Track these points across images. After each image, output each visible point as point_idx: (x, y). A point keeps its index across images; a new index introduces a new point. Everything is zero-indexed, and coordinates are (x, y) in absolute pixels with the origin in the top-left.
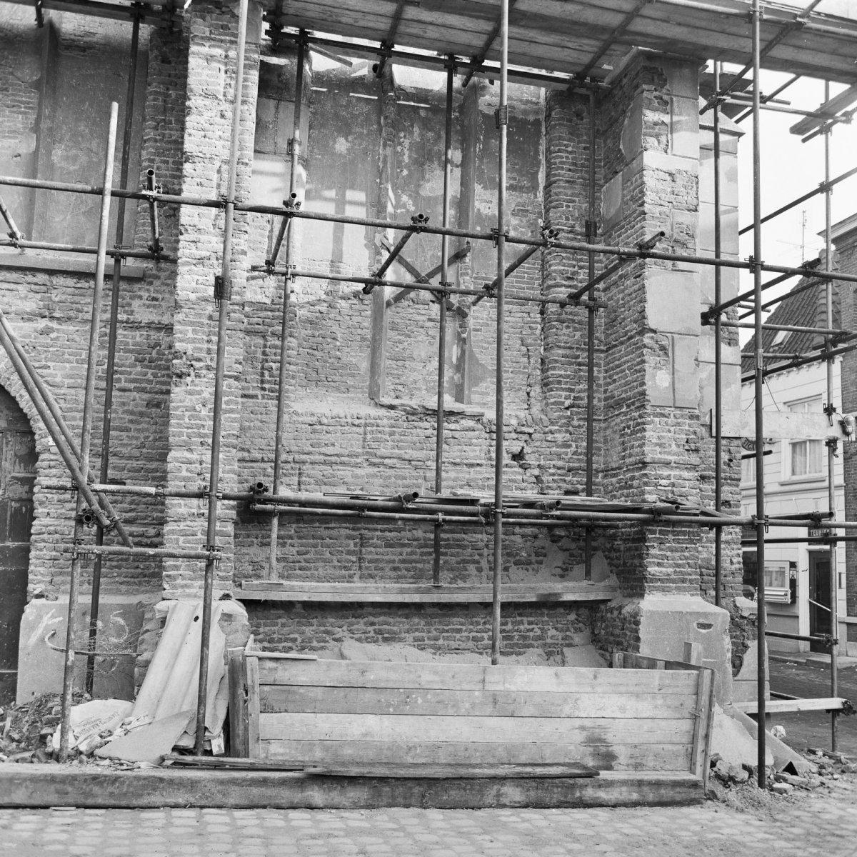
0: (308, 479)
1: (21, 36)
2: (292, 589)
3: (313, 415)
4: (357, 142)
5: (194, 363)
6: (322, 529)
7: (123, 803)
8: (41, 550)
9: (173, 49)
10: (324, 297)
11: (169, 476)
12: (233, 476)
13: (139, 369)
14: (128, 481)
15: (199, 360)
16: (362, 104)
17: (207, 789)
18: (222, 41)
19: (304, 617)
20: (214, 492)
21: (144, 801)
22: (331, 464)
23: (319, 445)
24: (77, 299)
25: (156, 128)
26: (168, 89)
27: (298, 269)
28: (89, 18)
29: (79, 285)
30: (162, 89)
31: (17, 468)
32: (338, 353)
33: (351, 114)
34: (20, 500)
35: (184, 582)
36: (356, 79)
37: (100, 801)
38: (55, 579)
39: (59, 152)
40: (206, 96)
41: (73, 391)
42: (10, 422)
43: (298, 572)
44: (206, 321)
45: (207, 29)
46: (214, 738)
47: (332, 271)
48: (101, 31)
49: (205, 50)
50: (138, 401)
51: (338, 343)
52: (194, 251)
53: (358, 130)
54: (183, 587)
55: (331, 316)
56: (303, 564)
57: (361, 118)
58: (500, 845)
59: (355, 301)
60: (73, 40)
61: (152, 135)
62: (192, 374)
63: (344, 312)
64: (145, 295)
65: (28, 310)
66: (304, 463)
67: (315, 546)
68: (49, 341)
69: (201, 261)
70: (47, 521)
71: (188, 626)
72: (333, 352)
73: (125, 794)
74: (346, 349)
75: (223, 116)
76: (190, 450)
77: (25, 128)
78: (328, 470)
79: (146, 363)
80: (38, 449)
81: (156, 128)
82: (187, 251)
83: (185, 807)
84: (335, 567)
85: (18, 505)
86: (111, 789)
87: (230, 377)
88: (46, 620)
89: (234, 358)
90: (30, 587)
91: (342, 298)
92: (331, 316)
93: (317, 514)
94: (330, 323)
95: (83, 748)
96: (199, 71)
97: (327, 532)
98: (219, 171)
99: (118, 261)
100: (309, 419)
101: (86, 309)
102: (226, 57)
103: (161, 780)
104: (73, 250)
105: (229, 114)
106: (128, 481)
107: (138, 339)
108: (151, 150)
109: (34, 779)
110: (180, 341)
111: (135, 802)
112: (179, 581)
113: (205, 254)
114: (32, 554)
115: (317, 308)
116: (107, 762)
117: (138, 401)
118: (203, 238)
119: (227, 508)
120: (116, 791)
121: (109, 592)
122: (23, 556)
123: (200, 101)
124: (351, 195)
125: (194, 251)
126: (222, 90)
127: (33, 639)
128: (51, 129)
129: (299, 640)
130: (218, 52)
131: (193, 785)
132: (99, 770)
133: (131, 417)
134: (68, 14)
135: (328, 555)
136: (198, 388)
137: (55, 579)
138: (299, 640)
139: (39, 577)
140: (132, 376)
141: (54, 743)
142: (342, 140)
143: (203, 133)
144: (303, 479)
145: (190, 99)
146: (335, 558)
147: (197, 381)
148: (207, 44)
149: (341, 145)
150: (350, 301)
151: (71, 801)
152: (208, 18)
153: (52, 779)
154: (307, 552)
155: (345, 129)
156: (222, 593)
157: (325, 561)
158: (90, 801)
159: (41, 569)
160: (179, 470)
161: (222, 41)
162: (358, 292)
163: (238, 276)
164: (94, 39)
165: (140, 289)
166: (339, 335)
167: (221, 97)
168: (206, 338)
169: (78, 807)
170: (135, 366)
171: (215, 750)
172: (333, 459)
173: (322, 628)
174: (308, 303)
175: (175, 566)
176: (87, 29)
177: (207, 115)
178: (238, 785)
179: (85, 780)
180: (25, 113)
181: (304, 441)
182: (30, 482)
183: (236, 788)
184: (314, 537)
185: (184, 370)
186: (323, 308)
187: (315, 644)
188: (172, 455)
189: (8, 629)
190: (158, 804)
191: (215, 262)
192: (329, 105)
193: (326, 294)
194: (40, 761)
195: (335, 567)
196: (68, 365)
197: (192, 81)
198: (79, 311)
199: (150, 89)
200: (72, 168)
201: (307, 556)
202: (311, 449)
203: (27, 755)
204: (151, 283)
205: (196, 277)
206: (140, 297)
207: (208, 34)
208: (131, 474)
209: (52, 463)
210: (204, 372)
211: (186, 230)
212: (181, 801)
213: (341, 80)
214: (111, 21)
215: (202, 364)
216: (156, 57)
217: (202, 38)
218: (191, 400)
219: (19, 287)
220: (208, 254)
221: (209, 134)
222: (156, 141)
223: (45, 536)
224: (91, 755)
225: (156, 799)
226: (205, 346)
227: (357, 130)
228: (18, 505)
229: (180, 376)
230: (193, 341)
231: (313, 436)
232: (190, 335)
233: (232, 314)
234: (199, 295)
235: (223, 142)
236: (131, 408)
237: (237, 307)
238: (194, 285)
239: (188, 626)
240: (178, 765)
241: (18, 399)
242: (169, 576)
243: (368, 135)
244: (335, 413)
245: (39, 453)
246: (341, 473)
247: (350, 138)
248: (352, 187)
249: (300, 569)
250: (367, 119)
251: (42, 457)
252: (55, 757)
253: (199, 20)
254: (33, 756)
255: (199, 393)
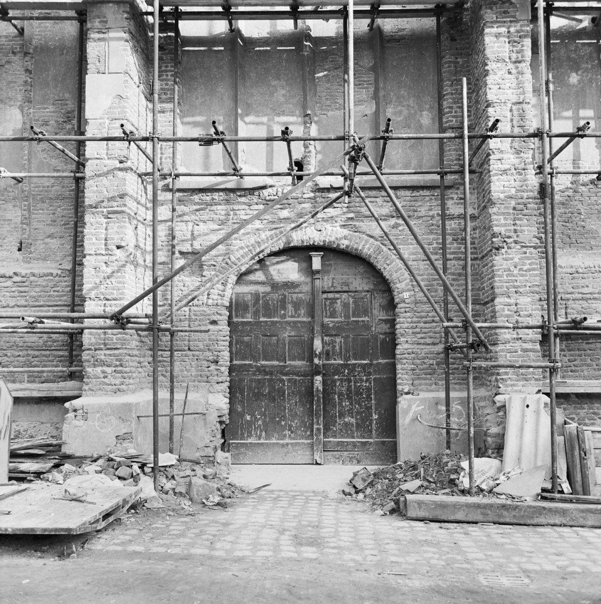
0: (572, 311)
1: (359, 39)
2: (573, 385)
3: (572, 267)
4: (584, 75)
5: (506, 239)
6: (584, 344)
7: (522, 522)
8: (404, 364)
9: (458, 30)
10: (570, 185)
11: (497, 314)
12: (538, 312)
13: (455, 245)
14: (455, 318)
15: (509, 237)
16: (586, 47)
17: (573, 515)
18: (505, 22)
19: (579, 404)
20: (552, 325)
21: (535, 521)
22: (587, 300)
23: (578, 287)
24: (413, 203)
25: (451, 85)
26: (456, 58)
27: (559, 170)
28: (400, 20)
29: (413, 195)
30: (453, 59)
31: (381, 313)
32: (583, 223)
33: (579, 55)
34: (385, 333)
35: (512, 383)
36: (580, 30)
37: (508, 520)
38: (415, 382)
39: (390, 110)
40: (498, 61)
41: (415, 263)
42: (375, 285)
43: (570, 373)
44: (512, 211)
45: (494, 16)
46: (563, 482)
47: (574, 167)
48: (408, 26)
49: (495, 30)
50: (457, 266)
51: (582, 217)
52: (500, 166)
53: (584, 66)
54: (512, 385)
55: (577, 198)
56: (573, 368)
57: (586, 57)
58: (584, 557)
59: (591, 186)
60: (392, 36)
61: (449, 91)
62: (506, 247)
63: (585, 194)
64: (455, 196)
65: (384, 214)
66: (568, 300)
67: (580, 356)
68: (398, 232)
69: (505, 172)
70: (406, 346)
71: (523, 411)
72: (579, 223)
73: (523, 516)
74: (588, 220)
75: (510, 73)
76: (509, 297)
77: (368, 97)
78: (585, 304)
79: (459, 241)
80: (396, 300)
81: (451, 85)
82: (496, 166)
83: (560, 526)
84: (595, 369)
85: (384, 337)
86: (514, 513)
87: (531, 247)
88: (414, 408)
89: (532, 234)
90: (399, 387)
91: (583, 185)
92: (577, 198)
93: (586, 334)
94: (576, 203)
95: (484, 486)
96: (492, 45)
97: (588, 346)
98: (511, 110)
99: (442, 177)
100: (570, 270)
101: (419, 209)
102: (509, 32)
103: (544, 508)
104: (415, 173)
105: (514, 71)
106: (455, 318)
107: (453, 226)
108: (450, 100)
109: (468, 506)
110: (497, 226)
111: (529, 522)
112: (509, 382)
113: (508, 167)
114: (399, 367)
115: (566, 193)
116: (503, 496)
117: (457, 266)
118: (505, 156)
119: (536, 334)
120: (517, 515)
121: (455, 390)
122: (393, 368)
123: (494, 65)
124: (583, 113)
125: (500, 166)
126: (507, 55)
127: (408, 420)
128: (384, 96)
129: (576, 419)
130: (503, 30)
131: (564, 512)
132: (499, 501)
133: (453, 277)
134: (387, 20)
135: (589, 361)
136: (510, 256)
137: (415, 382)
138: (576, 419)
139: (405, 381)
140: (452, 250)
141: (465, 483)
142: (574, 74)
143: (498, 86)
144: (569, 311)
145: (487, 65)
146: (594, 363)
147: (509, 251)
148: (495, 26)
149: (574, 78)
150: (588, 187)
151: (490, 519)
152: (494, 8)
153: (478, 506)
154: (575, 360)
155: (576, 67)
156: (537, 389)
157: (588, 365)
158: (502, 520)
159: (406, 376)
160: (503, 310)
161: (505, 22)
162: (594, 179)
163: (530, 179)
164: (405, 33)
165: (452, 193)
166: (582, 211)
167: (507, 60)
168: (512, 223)
169: (495, 523)
170: (453, 243)
171: (566, 491)
172: (588, 296)
173: (591, 411)
174: (560, 191)
175: (506, 372)
176: (400, 27)
177: (500, 73)
178: (593, 513)
179: (498, 507)
180: (366, 88)
181: (567, 285)
182: (392, 323)
183: (592, 515)
184: (579, 350)
185: (500, 245)
186: (570, 193)
187: (587, 421)
188: (497, 301)
189: (385, 414)
190: (544, 523)
191: (515, 172)
192: (563, 51)
193: (572, 183)
194: (458, 495)
195: (595, 369)
196: (411, 246)
197: (488, 52)
198: (416, 211)
199: (444, 60)
200: (399, 119)
201: (575, 363)
202: (573, 290)
203: (447, 491)
204: (458, 189)
205: (503, 183)
206: (452, 198)
207: (495, 19)
208: (456, 314)
209: (407, 309)
210: (513, 245)
211: (493, 152)
212: (557, 522)
213: (569, 33)
214: (414, 19)
215: (511, 240)
216: (447, 38)
217: (492, 22)
218: (507, 264)
219: (377, 200)
220: (509, 167)
221: (502, 86)
222: (452, 94)
223: (406, 356)
224: (490, 491)
225: (541, 520)
226: (512, 228)
227: (584, 66)
228: (384, 337)
229: (497, 249)
230: (505, 225)
231: (573, 281)
232: (503, 221)
233: (528, 205)
234: (506, 194)
235: (512, 90)
236: (452, 271)
237: (531, 200)
238: (502, 188)
239: (523, 411)
240: (544, 498)
241: (382, 270)
242: (502, 379)
243: (592, 68)
244: (587, 264)
245: (397, 304)
246: (594, 305)
247: (579, 73)
248: (584, 107)
249: (571, 371)
250: (591, 57)
251: (399, 306)
252: (463, 492)
253: (489, 11)
254: (452, 492)
255: (512, 259)
